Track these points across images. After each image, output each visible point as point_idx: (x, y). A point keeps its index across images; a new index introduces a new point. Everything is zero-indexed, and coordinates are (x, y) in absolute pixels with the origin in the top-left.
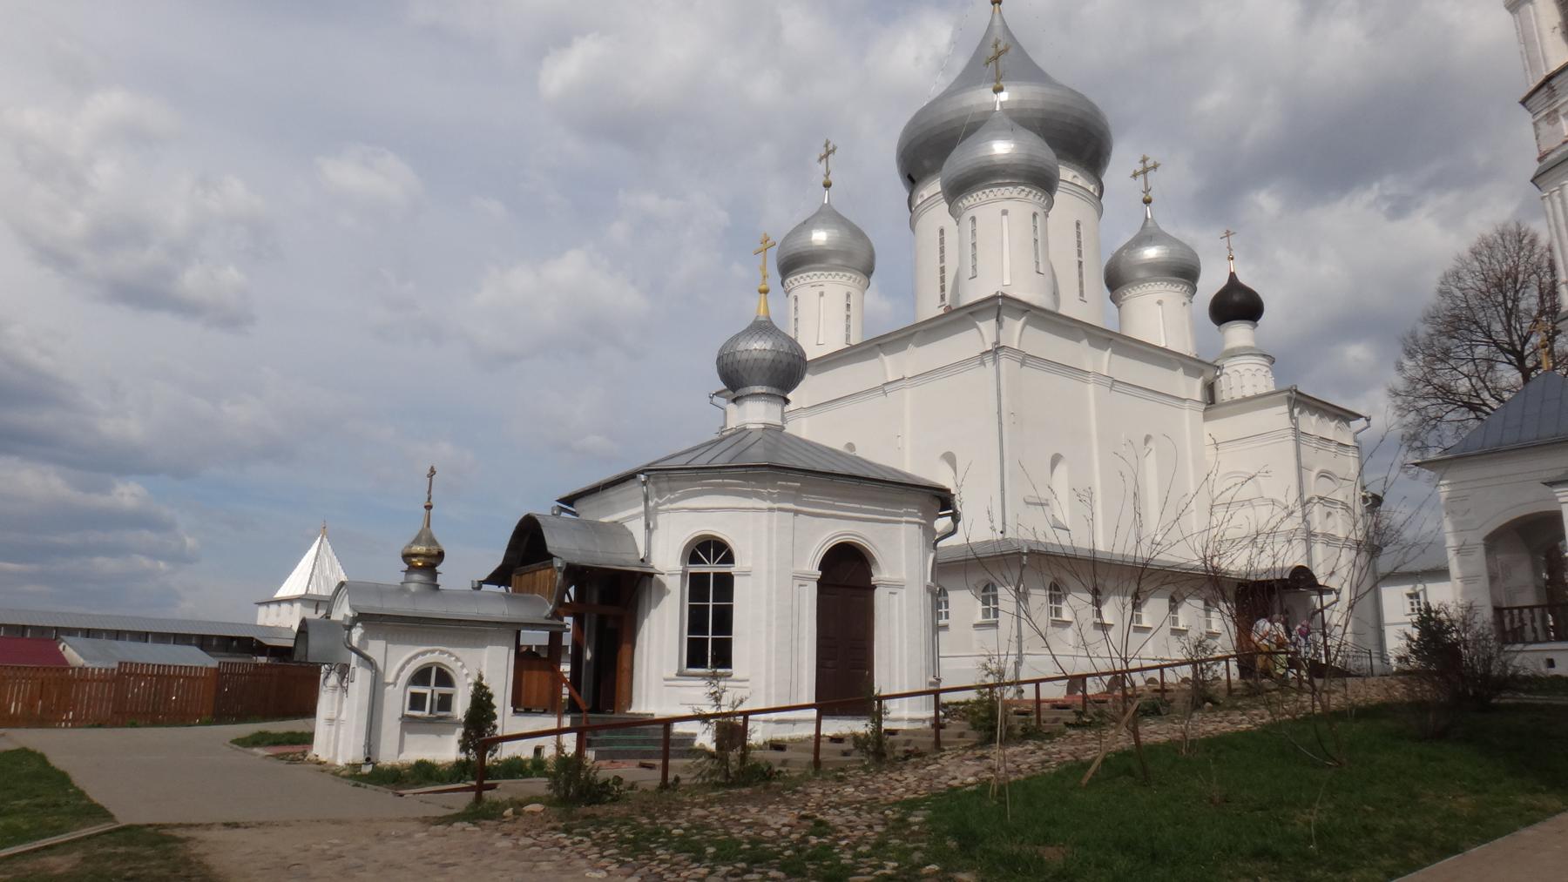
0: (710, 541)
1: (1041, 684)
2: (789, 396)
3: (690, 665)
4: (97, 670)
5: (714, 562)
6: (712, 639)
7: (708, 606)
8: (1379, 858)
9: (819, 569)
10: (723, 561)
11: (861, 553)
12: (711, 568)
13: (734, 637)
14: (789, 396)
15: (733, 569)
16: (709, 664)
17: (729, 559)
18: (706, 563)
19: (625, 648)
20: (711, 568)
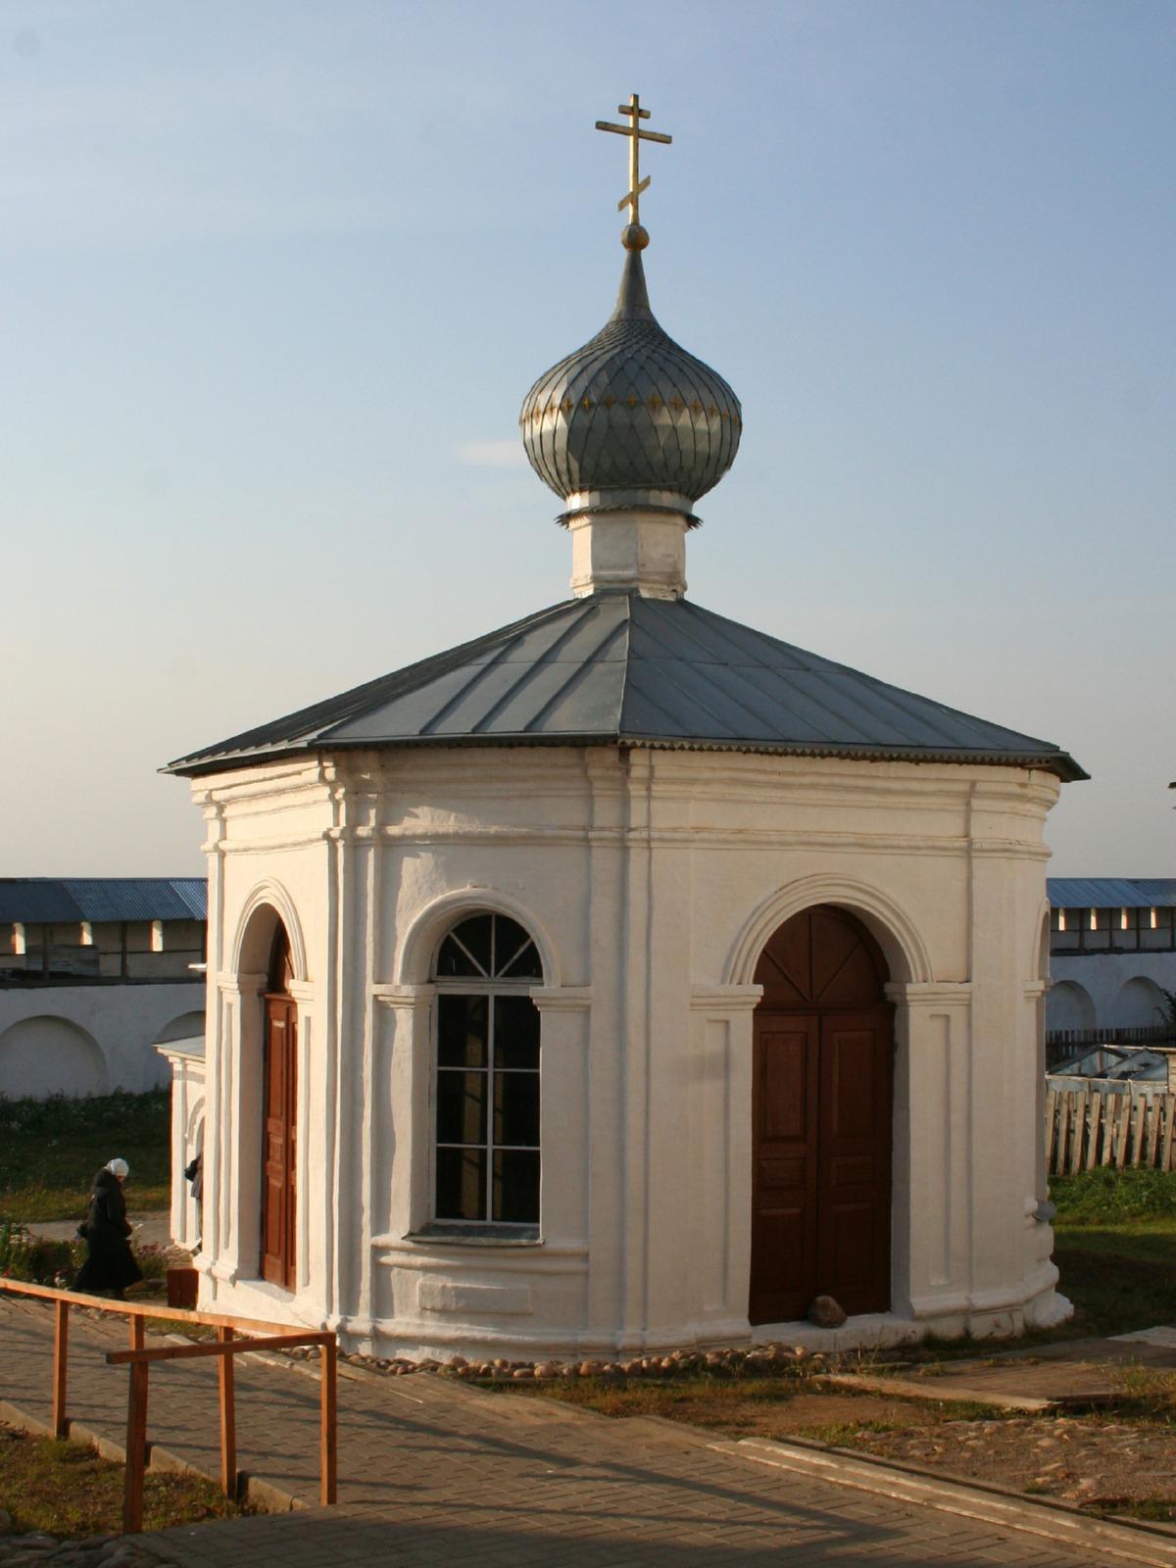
0: (490, 917)
1: (118, 973)
2: (698, 508)
3: (440, 1214)
4: (1076, 1033)
5: (496, 973)
6: (494, 1151)
7: (495, 1066)
8: (1137, 1420)
9: (756, 981)
10: (512, 973)
11: (866, 929)
12: (491, 987)
13: (435, 1069)
14: (698, 508)
15: (535, 992)
16: (443, 1068)
17: (530, 965)
18: (479, 974)
19: (293, 1173)
20: (491, 987)
